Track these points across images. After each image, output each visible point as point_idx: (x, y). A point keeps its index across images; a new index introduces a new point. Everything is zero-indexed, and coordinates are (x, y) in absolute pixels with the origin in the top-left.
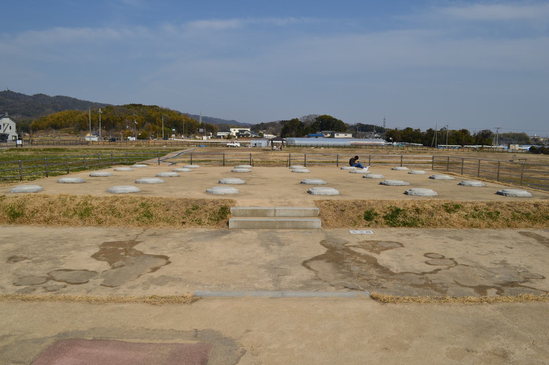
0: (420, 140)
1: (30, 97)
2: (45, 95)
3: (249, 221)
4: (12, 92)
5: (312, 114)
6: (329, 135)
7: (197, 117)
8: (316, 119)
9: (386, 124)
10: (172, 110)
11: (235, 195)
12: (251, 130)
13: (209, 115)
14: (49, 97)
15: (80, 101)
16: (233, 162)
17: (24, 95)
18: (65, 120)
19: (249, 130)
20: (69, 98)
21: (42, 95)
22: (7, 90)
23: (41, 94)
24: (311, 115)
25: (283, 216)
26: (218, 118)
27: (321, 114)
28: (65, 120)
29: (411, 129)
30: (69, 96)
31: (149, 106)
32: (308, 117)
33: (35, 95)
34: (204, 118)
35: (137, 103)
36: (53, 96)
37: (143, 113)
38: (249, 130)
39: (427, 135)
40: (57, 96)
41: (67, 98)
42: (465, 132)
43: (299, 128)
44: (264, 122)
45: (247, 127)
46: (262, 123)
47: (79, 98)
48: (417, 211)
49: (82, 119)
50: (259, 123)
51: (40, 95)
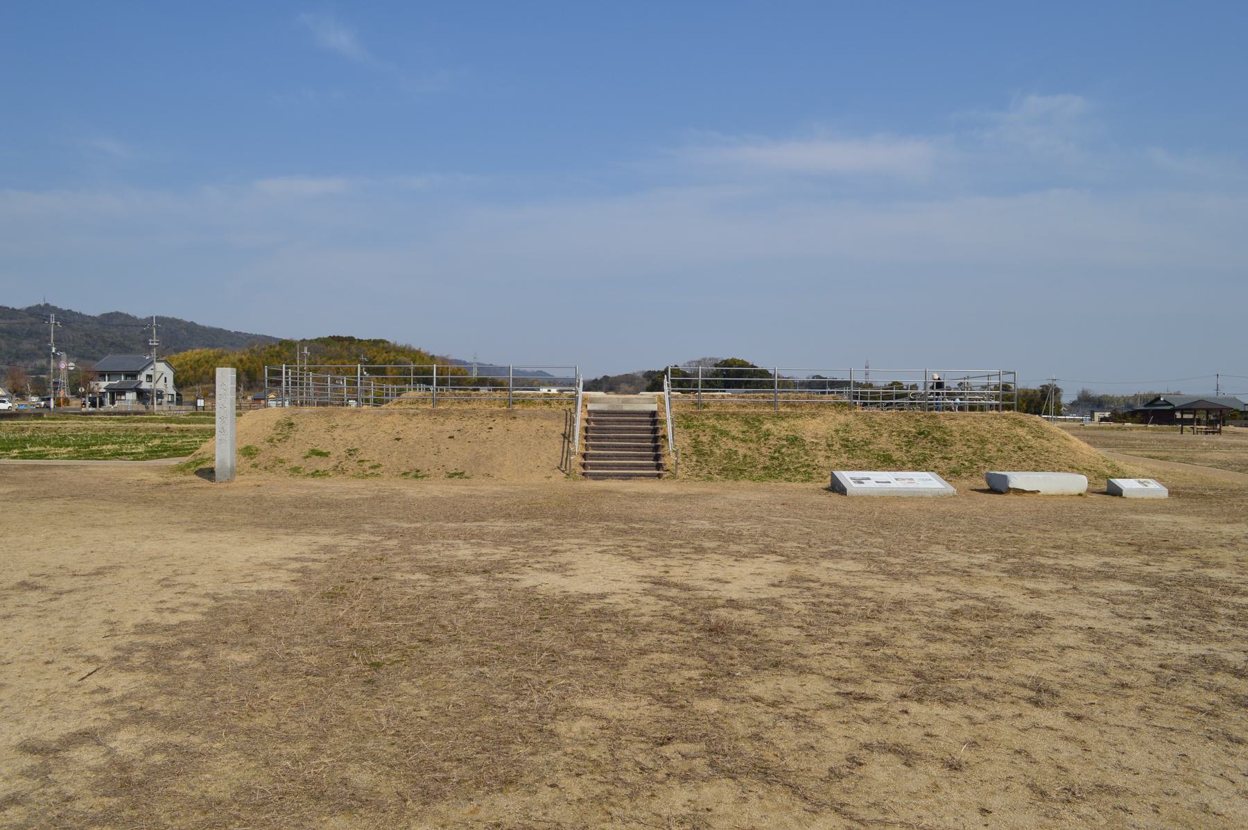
1: (94, 318)
2: (127, 316)
3: (898, 498)
9: (1222, 391)
11: (564, 516)
14: (135, 318)
15: (204, 329)
18: (195, 370)
20: (179, 322)
22: (42, 304)
23: (117, 313)
28: (195, 370)
30: (178, 317)
31: (369, 341)
34: (481, 368)
44: (611, 375)
46: (606, 378)
50: (599, 376)
51: (117, 315)
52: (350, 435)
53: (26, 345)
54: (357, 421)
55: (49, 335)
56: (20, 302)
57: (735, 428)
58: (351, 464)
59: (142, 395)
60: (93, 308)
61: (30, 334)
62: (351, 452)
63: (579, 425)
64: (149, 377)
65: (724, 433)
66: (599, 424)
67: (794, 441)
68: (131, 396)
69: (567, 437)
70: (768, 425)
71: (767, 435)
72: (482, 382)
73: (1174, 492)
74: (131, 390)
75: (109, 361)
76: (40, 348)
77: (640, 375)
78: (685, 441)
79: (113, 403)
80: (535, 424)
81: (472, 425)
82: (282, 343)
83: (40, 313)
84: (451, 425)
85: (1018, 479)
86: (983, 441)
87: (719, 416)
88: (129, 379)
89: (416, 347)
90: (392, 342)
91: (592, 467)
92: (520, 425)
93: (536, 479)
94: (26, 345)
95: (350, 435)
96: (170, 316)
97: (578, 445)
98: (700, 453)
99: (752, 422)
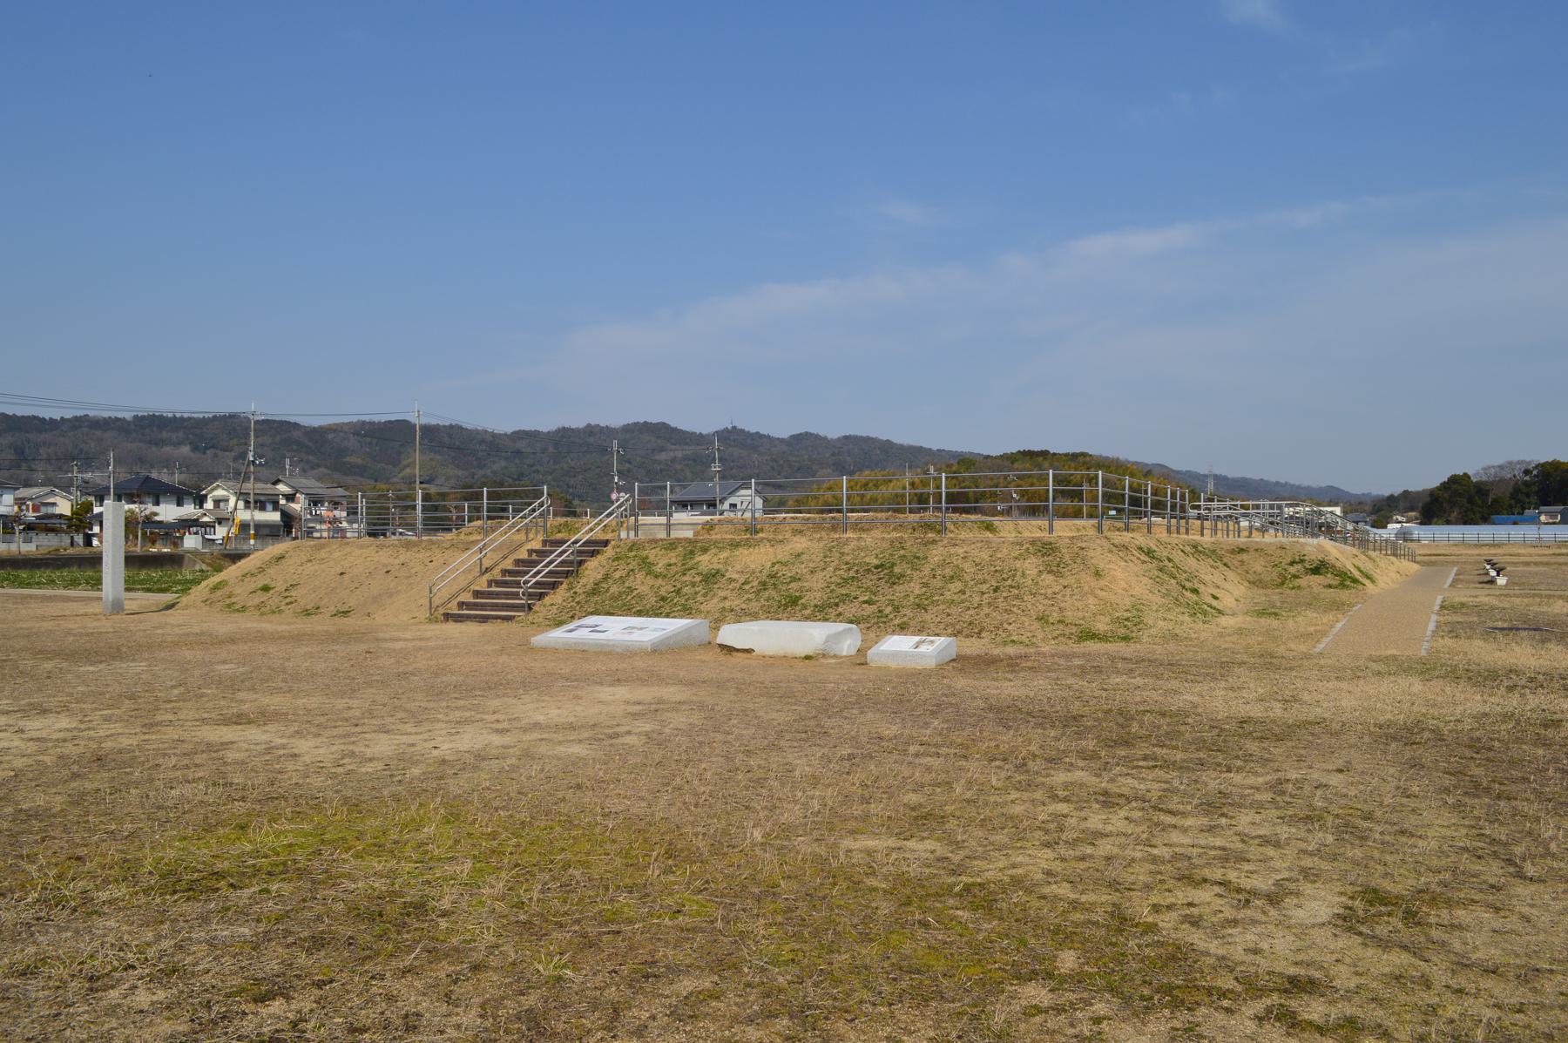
1: (781, 441)
4: (742, 431)
5: (1515, 458)
12: (1345, 512)
15: (901, 447)
16: (148, 590)
19: (1338, 510)
24: (1510, 463)
32: (1501, 467)
33: (794, 437)
35: (1036, 447)
38: (1338, 510)
40: (846, 437)
41: (868, 440)
43: (1470, 501)
46: (1406, 492)
47: (898, 439)
48: (354, 806)
50: (1397, 491)
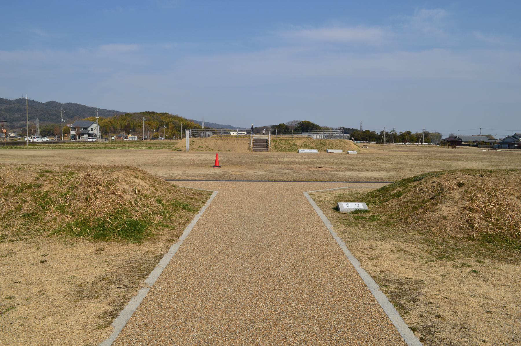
0: (374, 139)
1: (43, 104)
2: (57, 102)
5: (296, 120)
6: (306, 136)
7: (201, 123)
8: (298, 124)
10: (434, 132)
13: (211, 121)
15: (89, 108)
17: (37, 102)
21: (55, 102)
25: (236, 180)
26: (214, 123)
27: (303, 120)
29: (369, 131)
32: (292, 122)
36: (64, 103)
37: (157, 119)
38: (245, 133)
39: (398, 136)
40: (68, 103)
41: (76, 105)
42: (409, 133)
45: (244, 131)
49: (106, 124)
52: (206, 144)
53: (17, 115)
54: (207, 141)
55: (25, 111)
56: (11, 95)
57: (283, 142)
58: (208, 149)
59: (90, 136)
60: (43, 99)
61: (18, 110)
62: (207, 147)
63: (252, 141)
64: (92, 129)
65: (281, 143)
66: (256, 141)
67: (295, 145)
68: (86, 136)
69: (249, 144)
70: (290, 142)
71: (289, 143)
72: (208, 129)
73: (229, 133)
74: (86, 134)
75: (77, 123)
76: (23, 117)
77: (270, 127)
78: (273, 145)
79: (79, 138)
80: (243, 141)
81: (230, 141)
82: (127, 114)
83: (21, 101)
84: (226, 142)
85: (330, 151)
86: (333, 145)
87: (280, 140)
88: (85, 130)
89: (180, 116)
90: (170, 114)
91: (255, 149)
92: (240, 141)
93: (244, 151)
94: (17, 115)
95: (206, 144)
96: (75, 102)
97: (252, 145)
98: (276, 147)
99: (287, 141)
